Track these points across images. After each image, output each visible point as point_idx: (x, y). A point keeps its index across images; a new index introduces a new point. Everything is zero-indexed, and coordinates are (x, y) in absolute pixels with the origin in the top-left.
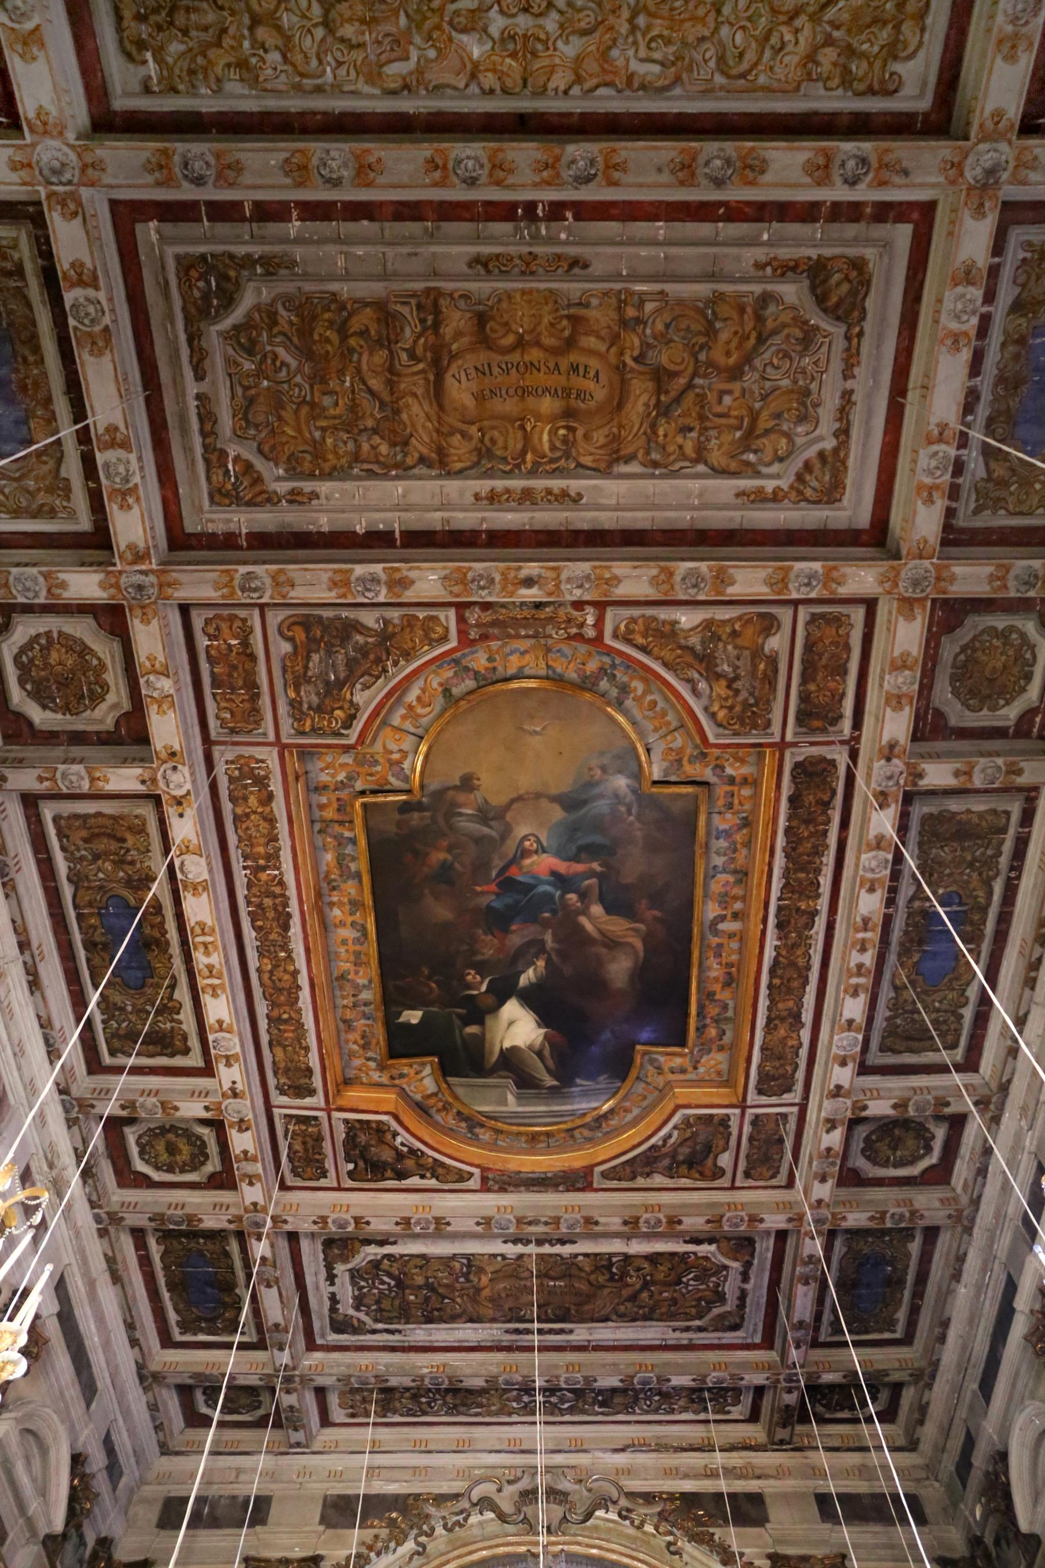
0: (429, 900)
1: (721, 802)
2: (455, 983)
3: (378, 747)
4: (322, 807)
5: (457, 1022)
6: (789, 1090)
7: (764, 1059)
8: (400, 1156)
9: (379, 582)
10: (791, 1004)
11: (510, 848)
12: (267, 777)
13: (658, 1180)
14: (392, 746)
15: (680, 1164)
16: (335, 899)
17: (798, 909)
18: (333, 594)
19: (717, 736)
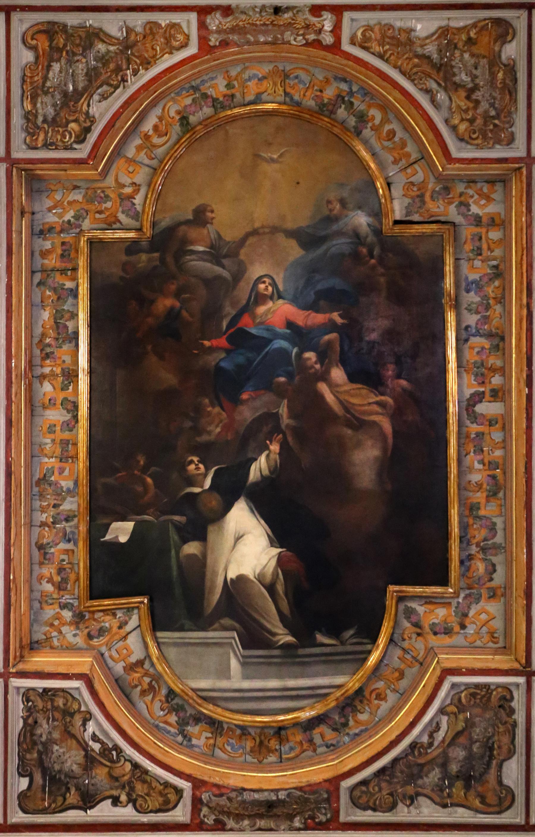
1: (468, 247)
2: (175, 476)
3: (110, 181)
4: (44, 254)
5: (174, 536)
11: (243, 292)
14: (125, 179)
16: (47, 370)
19: (459, 150)
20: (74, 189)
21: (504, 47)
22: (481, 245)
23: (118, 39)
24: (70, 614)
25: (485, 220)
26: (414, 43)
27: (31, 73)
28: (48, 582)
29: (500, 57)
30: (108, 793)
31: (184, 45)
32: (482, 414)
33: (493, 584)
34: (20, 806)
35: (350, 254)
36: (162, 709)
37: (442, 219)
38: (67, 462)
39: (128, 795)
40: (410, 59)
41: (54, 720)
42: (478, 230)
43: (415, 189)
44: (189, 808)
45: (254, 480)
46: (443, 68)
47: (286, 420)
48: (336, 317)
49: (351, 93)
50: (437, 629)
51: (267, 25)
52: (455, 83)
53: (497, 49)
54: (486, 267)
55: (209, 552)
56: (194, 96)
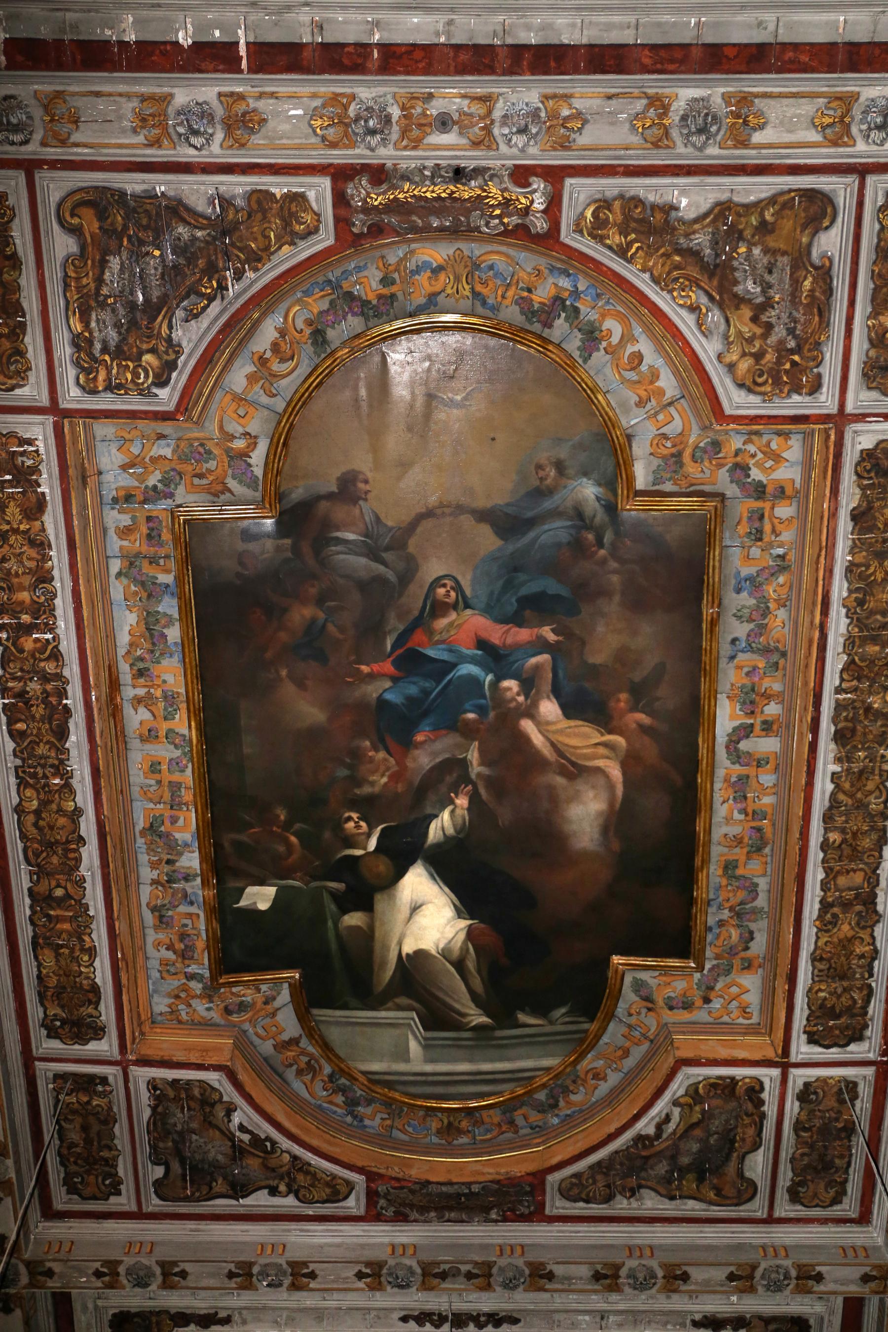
0: (289, 689)
2: (327, 835)
6: (858, 1037)
7: (818, 977)
8: (238, 1152)
9: (211, 118)
10: (858, 878)
11: (414, 599)
12: (35, 470)
13: (651, 1203)
15: (683, 1171)
17: (868, 709)
18: (140, 139)
20: (158, 439)
21: (816, 239)
22: (762, 527)
23: (208, 218)
24: (200, 986)
25: (770, 489)
26: (674, 229)
27: (76, 272)
28: (167, 949)
29: (809, 253)
30: (263, 1184)
31: (312, 231)
32: (748, 753)
33: (748, 954)
34: (156, 1192)
35: (569, 543)
36: (325, 1090)
37: (707, 488)
38: (181, 809)
39: (288, 1186)
40: (666, 255)
41: (189, 1109)
42: (759, 504)
43: (669, 444)
44: (363, 1200)
45: (435, 841)
46: (718, 271)
47: (476, 768)
48: (548, 633)
49: (576, 293)
50: (674, 1003)
51: (444, 199)
52: (736, 295)
53: (804, 240)
54: (768, 557)
55: (377, 924)
56: (333, 297)
